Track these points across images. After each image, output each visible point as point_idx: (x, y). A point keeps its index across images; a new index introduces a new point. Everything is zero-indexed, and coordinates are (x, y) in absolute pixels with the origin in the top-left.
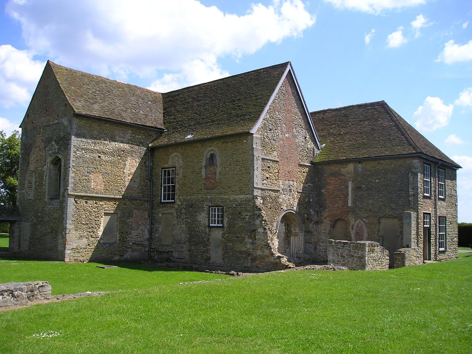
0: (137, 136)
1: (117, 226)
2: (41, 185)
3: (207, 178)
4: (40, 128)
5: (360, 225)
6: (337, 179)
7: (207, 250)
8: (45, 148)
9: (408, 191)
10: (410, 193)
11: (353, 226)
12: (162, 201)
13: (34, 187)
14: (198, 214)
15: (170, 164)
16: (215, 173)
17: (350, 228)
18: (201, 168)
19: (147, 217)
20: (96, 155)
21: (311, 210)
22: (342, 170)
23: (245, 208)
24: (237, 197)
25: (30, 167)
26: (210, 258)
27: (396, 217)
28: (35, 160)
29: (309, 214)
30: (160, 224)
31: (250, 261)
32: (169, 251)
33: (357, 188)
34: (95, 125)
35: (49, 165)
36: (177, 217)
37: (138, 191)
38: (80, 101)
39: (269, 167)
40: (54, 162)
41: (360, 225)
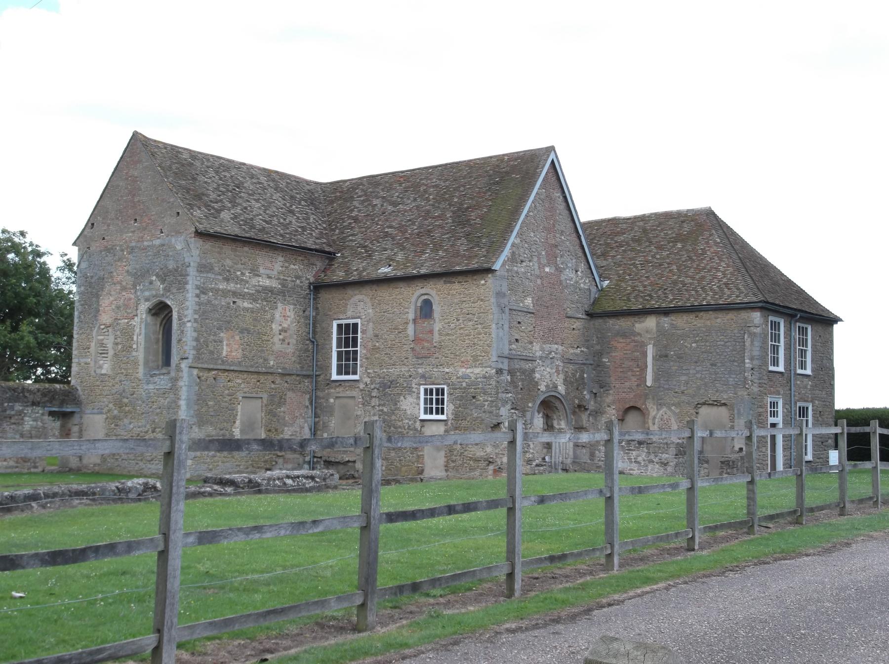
0: (292, 266)
1: (262, 418)
2: (128, 348)
3: (417, 340)
4: (123, 251)
5: (665, 417)
6: (628, 340)
7: (419, 456)
8: (134, 286)
9: (744, 363)
10: (747, 365)
11: (654, 418)
12: (335, 377)
13: (111, 353)
14: (402, 398)
15: (349, 313)
16: (431, 332)
17: (650, 421)
18: (407, 323)
19: (307, 403)
20: (230, 300)
21: (585, 393)
22: (637, 325)
23: (482, 388)
24: (469, 371)
25: (100, 318)
26: (423, 471)
27: (725, 404)
28: (113, 307)
29: (582, 399)
30: (332, 415)
31: (491, 472)
32: (349, 461)
33: (661, 357)
34: (228, 249)
35: (144, 316)
36: (363, 404)
37: (293, 359)
38: (199, 208)
39: (519, 323)
40: (153, 311)
41: (665, 417)
